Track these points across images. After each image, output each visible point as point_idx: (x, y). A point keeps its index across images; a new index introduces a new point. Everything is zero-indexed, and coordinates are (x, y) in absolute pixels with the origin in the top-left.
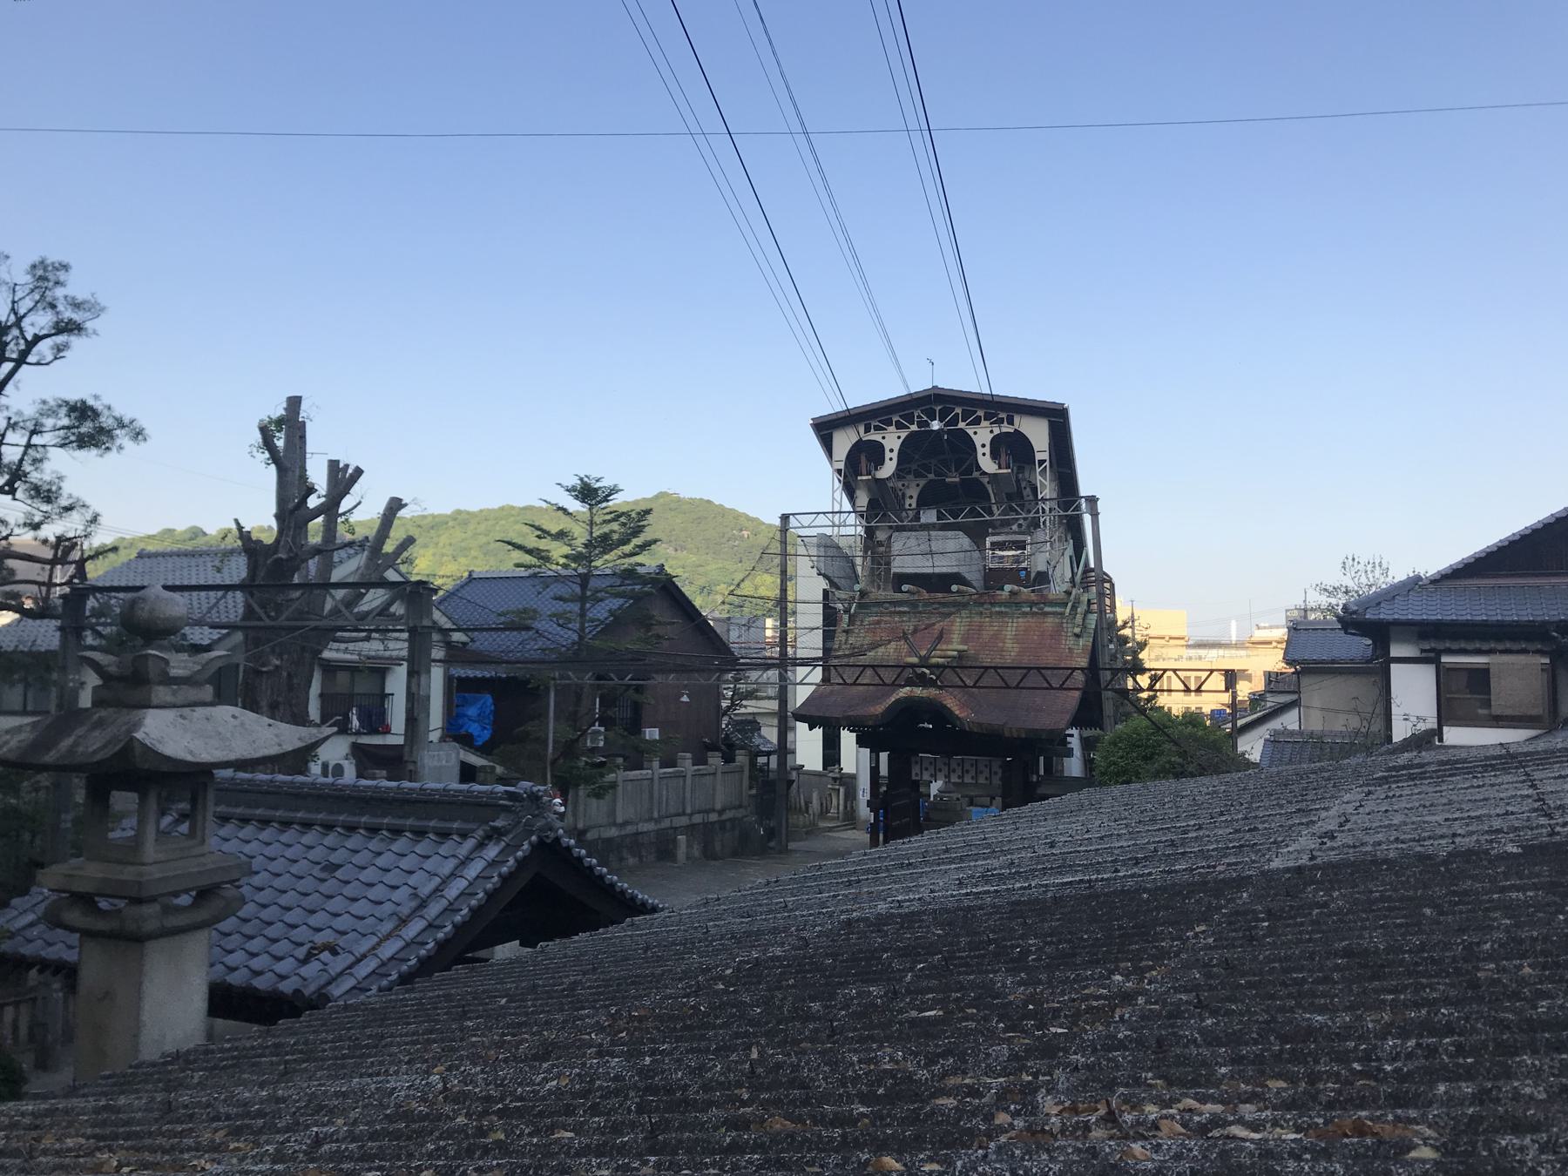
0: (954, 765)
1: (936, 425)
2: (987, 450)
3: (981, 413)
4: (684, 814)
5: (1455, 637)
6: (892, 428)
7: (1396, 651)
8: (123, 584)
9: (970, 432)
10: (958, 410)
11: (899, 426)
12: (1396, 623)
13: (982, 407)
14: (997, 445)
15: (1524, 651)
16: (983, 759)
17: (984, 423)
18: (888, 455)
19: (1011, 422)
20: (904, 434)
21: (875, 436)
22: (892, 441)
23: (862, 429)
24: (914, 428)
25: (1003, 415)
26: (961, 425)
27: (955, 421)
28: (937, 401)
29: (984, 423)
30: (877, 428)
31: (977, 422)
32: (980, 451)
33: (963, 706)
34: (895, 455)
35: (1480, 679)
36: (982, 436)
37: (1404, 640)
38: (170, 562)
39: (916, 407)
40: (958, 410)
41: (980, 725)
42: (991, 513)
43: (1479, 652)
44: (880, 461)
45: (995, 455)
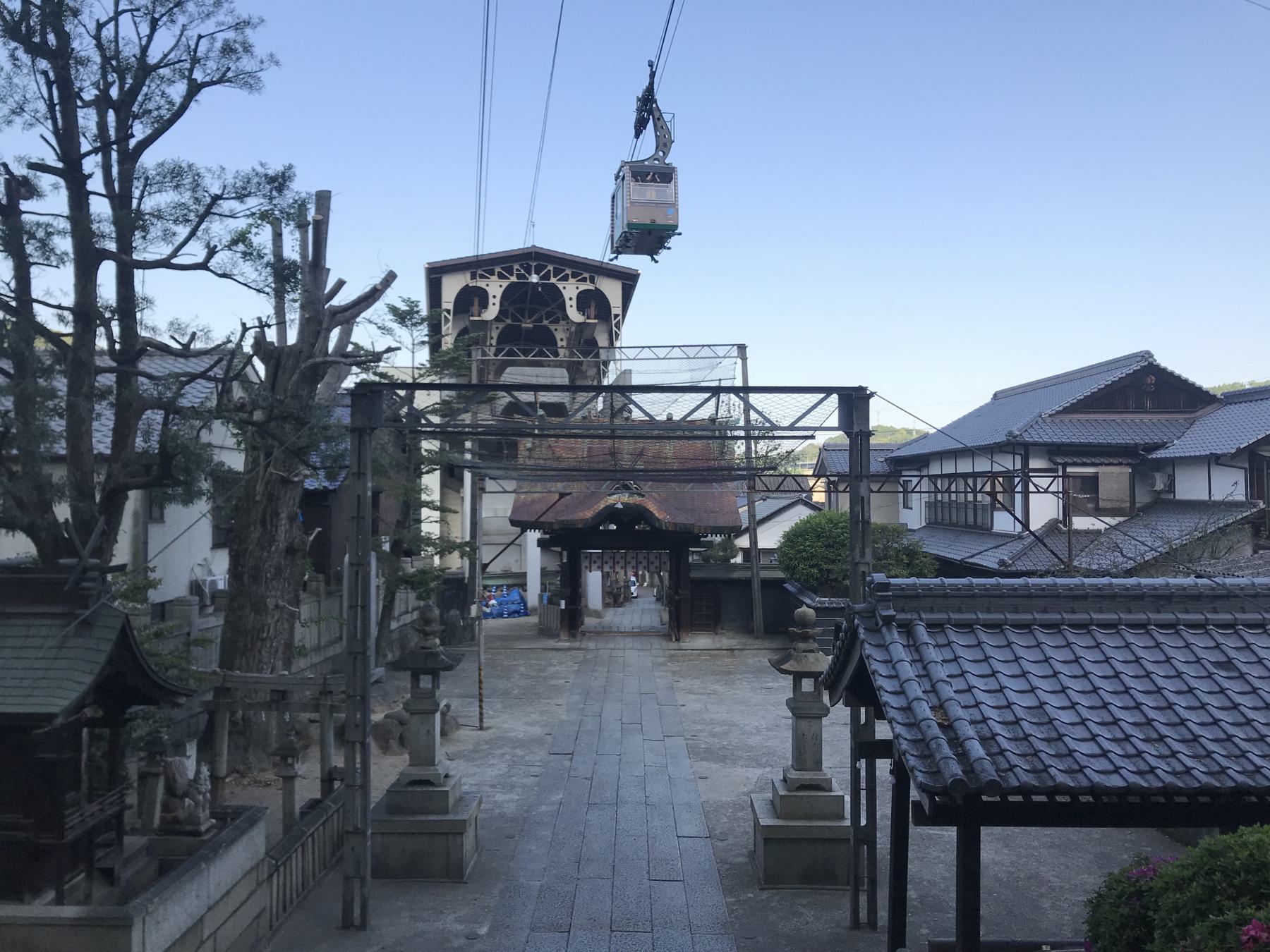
0: (618, 557)
1: (534, 278)
2: (574, 303)
3: (568, 271)
4: (407, 612)
5: (1073, 454)
6: (495, 278)
7: (1034, 464)
8: (912, 868)
9: (560, 286)
10: (550, 268)
11: (501, 276)
12: (1035, 444)
13: (570, 267)
14: (584, 301)
15: (1120, 464)
16: (631, 553)
17: (571, 280)
18: (491, 300)
19: (592, 281)
20: (505, 284)
21: (481, 284)
22: (495, 288)
23: (468, 275)
24: (514, 279)
25: (586, 275)
26: (553, 280)
27: (547, 276)
28: (534, 258)
29: (571, 280)
30: (482, 277)
31: (565, 278)
32: (568, 303)
33: (660, 510)
34: (497, 301)
35: (1091, 483)
36: (570, 290)
37: (1039, 456)
38: (230, 924)
39: (516, 261)
40: (550, 268)
41: (675, 524)
42: (557, 355)
43: (1084, 465)
44: (484, 304)
45: (581, 307)
